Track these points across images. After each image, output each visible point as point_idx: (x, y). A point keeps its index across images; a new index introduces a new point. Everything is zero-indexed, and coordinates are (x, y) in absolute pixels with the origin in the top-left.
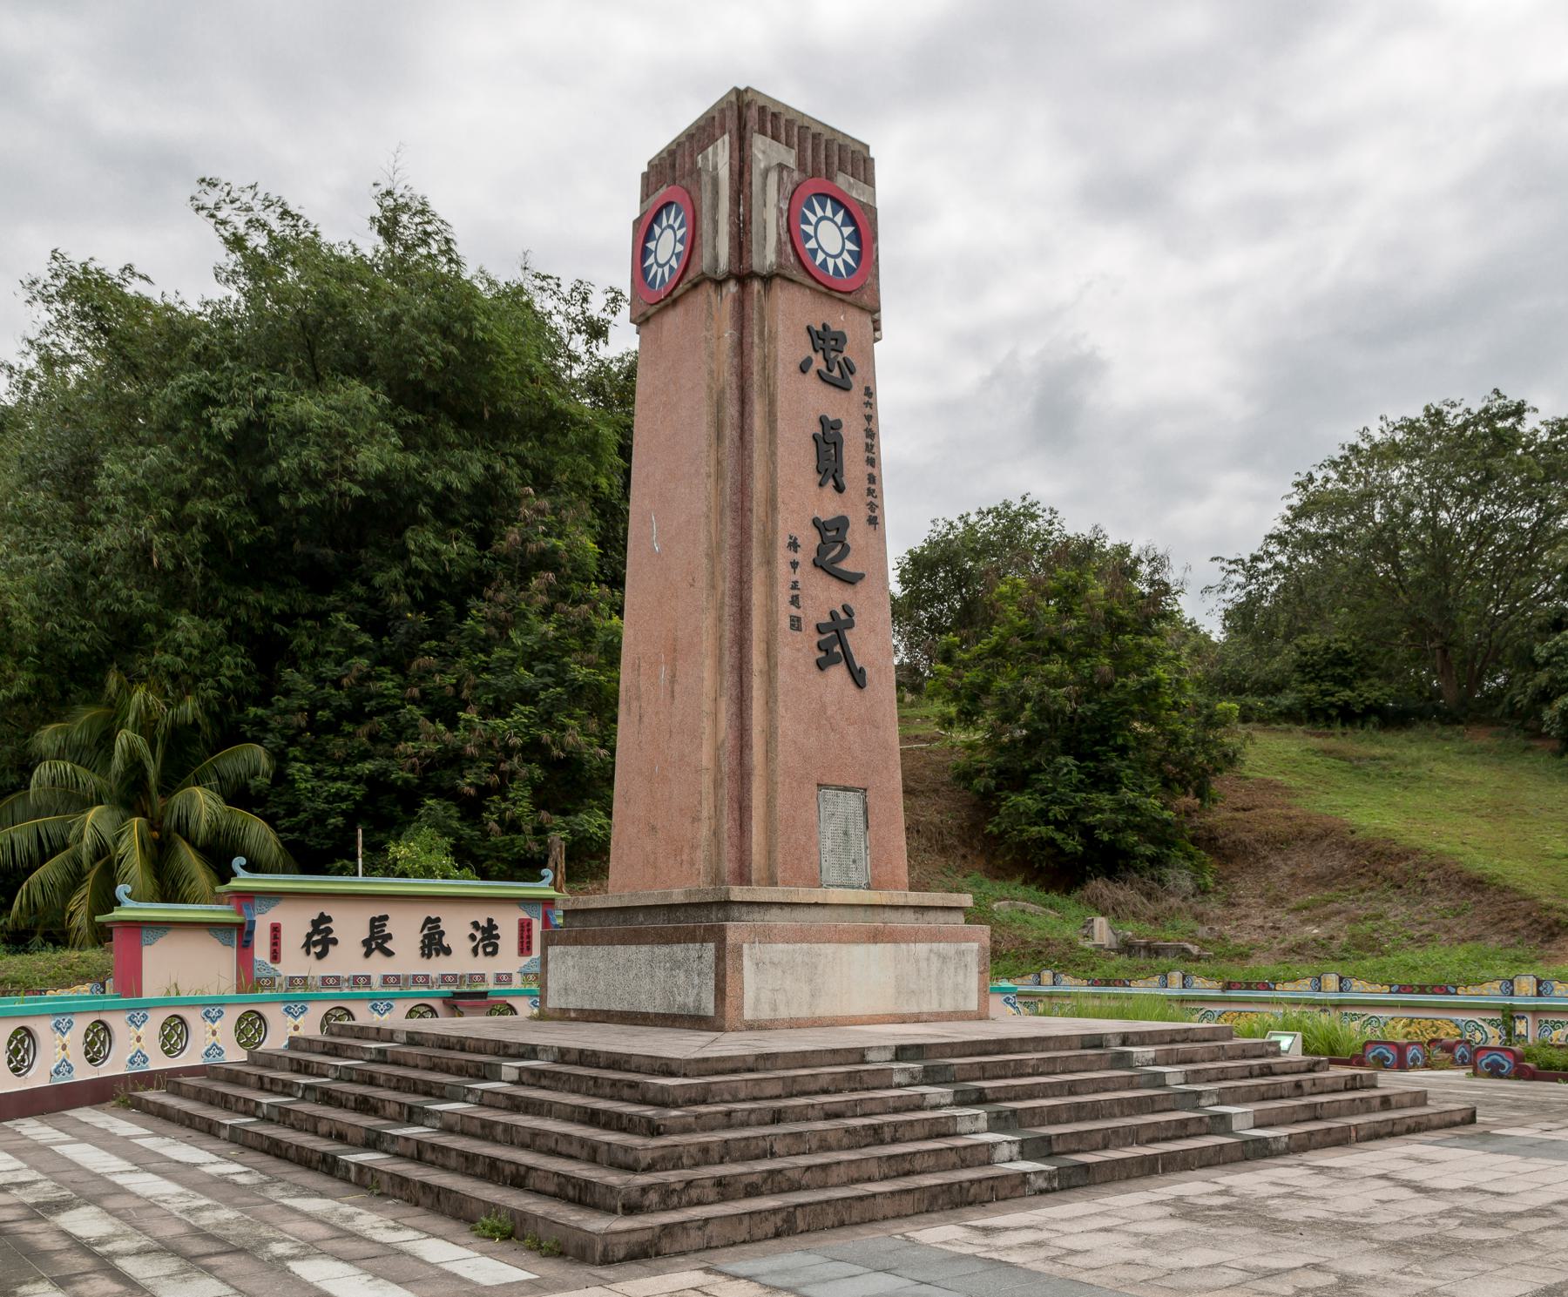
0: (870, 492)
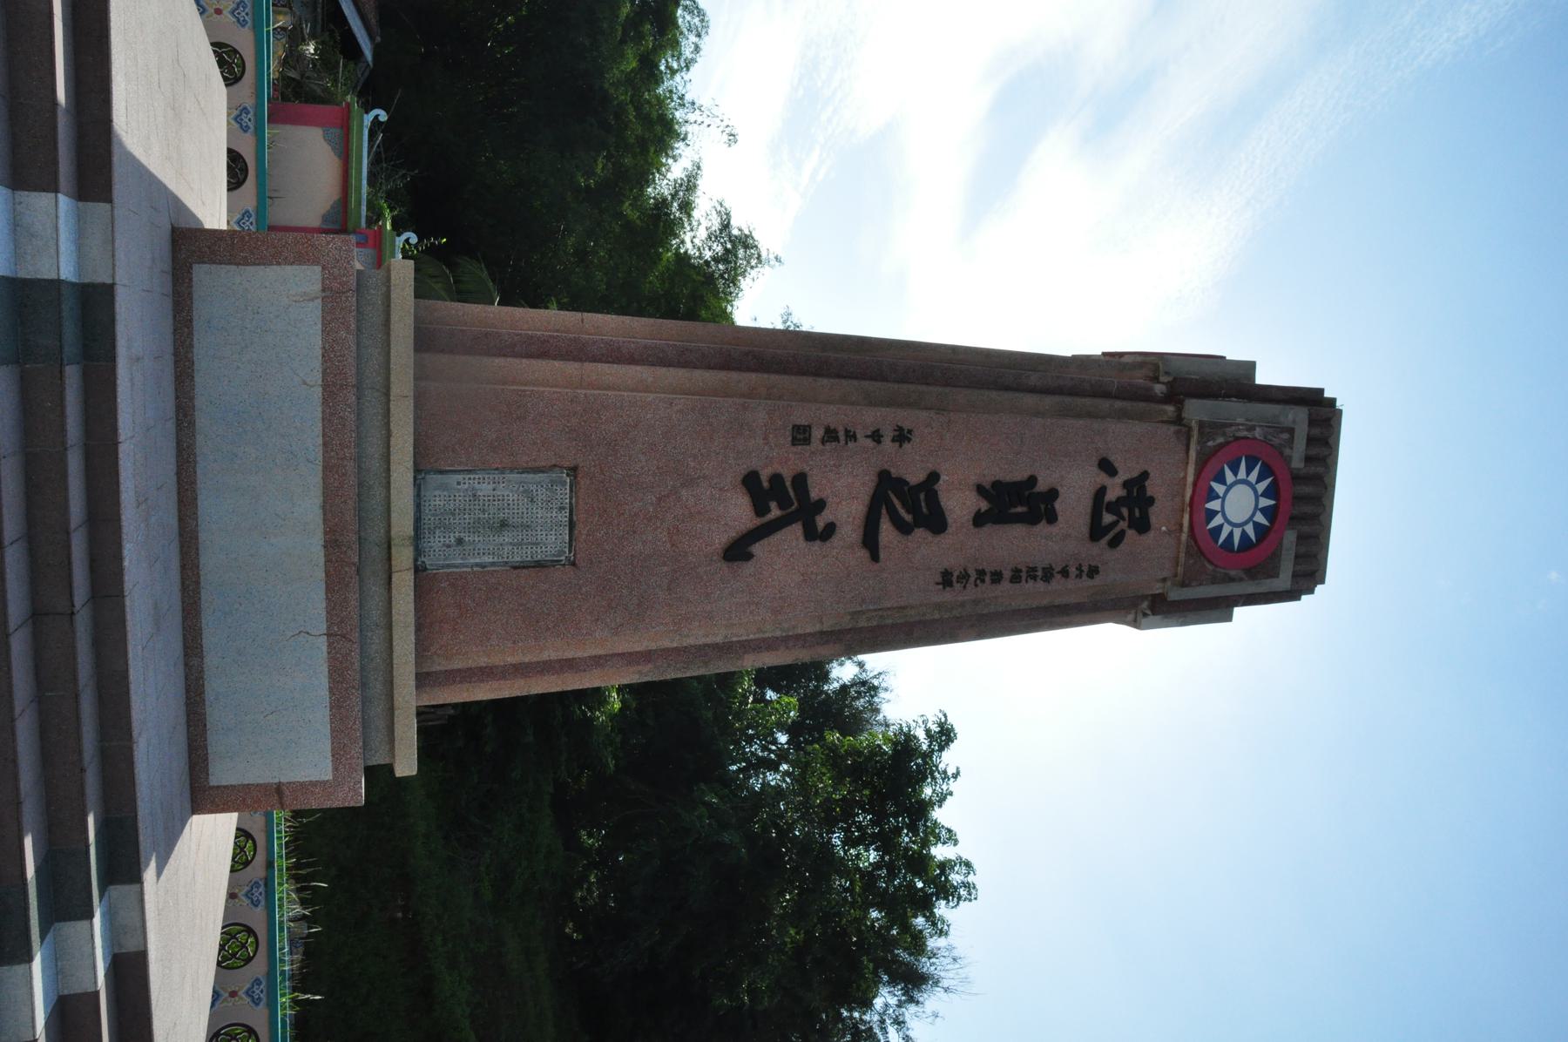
0: (981, 573)
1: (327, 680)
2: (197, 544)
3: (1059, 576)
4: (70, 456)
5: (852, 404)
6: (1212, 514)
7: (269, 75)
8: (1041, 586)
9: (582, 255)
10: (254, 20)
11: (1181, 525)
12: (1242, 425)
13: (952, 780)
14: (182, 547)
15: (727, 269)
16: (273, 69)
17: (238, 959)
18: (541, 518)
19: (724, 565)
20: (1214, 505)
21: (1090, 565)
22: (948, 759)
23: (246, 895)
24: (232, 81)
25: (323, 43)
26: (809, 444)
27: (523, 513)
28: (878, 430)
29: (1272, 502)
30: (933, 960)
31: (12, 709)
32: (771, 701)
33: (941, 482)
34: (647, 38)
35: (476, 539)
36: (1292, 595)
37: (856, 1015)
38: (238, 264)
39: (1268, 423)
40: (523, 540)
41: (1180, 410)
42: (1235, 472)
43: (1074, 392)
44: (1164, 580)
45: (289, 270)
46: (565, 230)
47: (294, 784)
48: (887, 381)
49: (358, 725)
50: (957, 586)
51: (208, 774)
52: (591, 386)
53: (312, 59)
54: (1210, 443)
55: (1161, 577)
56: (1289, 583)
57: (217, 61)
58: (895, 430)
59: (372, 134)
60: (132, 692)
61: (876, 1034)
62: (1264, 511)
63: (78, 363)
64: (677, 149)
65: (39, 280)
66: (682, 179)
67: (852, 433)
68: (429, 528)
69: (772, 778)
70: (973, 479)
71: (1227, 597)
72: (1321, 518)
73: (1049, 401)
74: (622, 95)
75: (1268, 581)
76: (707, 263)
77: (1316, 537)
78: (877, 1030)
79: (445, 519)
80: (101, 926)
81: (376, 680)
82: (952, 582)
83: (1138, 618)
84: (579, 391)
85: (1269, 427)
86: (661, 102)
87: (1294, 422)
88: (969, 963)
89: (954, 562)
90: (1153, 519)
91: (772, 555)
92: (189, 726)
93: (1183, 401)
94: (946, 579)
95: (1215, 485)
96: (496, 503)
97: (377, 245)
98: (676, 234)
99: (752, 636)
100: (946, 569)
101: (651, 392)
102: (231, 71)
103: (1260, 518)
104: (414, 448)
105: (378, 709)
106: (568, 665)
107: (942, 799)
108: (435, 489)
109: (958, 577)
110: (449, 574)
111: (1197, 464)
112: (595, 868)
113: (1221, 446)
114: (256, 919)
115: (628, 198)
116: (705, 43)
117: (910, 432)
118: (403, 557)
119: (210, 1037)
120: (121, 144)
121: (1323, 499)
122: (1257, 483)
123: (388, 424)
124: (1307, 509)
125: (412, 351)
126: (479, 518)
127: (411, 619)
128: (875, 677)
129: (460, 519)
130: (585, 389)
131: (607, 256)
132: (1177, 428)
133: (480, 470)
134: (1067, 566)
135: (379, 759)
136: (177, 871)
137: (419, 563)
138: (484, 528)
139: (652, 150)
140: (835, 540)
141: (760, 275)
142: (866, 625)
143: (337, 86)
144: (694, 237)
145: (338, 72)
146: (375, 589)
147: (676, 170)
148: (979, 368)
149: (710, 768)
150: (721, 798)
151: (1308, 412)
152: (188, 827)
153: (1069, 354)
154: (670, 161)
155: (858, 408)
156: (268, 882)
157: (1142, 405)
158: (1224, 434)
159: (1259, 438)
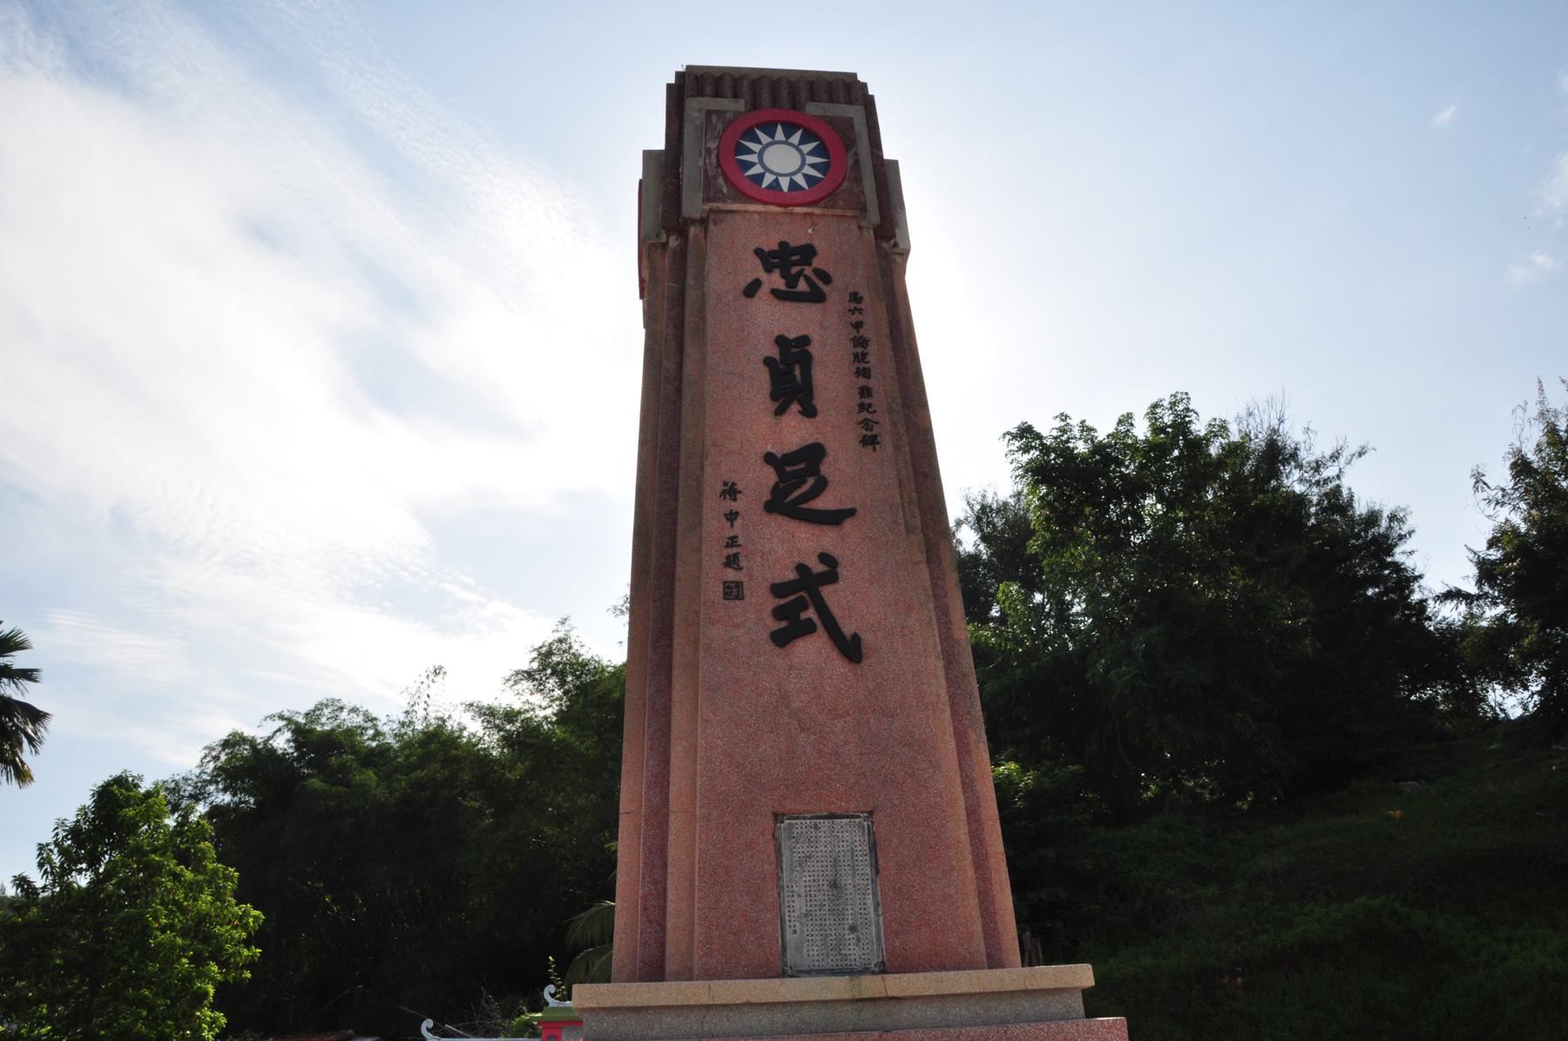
0: (863, 407)
3: (861, 331)
5: (700, 541)
6: (794, 185)
8: (872, 348)
9: (561, 819)
11: (806, 214)
13: (1068, 421)
15: (572, 673)
18: (826, 847)
19: (866, 663)
20: (785, 184)
21: (850, 301)
22: (1046, 428)
26: (742, 583)
27: (822, 866)
28: (725, 515)
30: (1252, 436)
33: (774, 451)
35: (850, 912)
36: (869, 104)
37: (1313, 510)
41: (693, 221)
42: (751, 165)
44: (860, 228)
46: (537, 837)
49: (1044, 1026)
50: (876, 431)
54: (725, 190)
55: (857, 230)
58: (725, 498)
61: (1331, 489)
62: (788, 135)
64: (453, 727)
66: (483, 721)
67: (730, 542)
68: (841, 960)
70: (769, 419)
72: (793, 79)
73: (690, 349)
74: (401, 784)
75: (856, 127)
82: (871, 436)
83: (900, 251)
84: (698, 813)
85: (706, 135)
86: (408, 745)
87: (700, 111)
88: (1252, 399)
89: (851, 436)
90: (802, 241)
93: (684, 218)
96: (813, 893)
99: (936, 632)
100: (860, 442)
103: (795, 139)
104: (761, 978)
105: (1026, 1006)
106: (973, 813)
107: (1086, 429)
108: (802, 957)
111: (745, 202)
113: (727, 180)
115: (504, 774)
116: (348, 702)
117: (725, 484)
118: (872, 986)
123: (738, 1006)
124: (784, 94)
127: (935, 975)
128: (972, 509)
131: (562, 794)
132: (711, 224)
133: (780, 910)
134: (851, 324)
135: (1078, 1004)
137: (877, 969)
139: (454, 752)
140: (829, 549)
146: (905, 1013)
147: (474, 727)
150: (1101, 656)
151: (690, 99)
154: (465, 733)
155: (704, 535)
157: (690, 260)
158: (715, 178)
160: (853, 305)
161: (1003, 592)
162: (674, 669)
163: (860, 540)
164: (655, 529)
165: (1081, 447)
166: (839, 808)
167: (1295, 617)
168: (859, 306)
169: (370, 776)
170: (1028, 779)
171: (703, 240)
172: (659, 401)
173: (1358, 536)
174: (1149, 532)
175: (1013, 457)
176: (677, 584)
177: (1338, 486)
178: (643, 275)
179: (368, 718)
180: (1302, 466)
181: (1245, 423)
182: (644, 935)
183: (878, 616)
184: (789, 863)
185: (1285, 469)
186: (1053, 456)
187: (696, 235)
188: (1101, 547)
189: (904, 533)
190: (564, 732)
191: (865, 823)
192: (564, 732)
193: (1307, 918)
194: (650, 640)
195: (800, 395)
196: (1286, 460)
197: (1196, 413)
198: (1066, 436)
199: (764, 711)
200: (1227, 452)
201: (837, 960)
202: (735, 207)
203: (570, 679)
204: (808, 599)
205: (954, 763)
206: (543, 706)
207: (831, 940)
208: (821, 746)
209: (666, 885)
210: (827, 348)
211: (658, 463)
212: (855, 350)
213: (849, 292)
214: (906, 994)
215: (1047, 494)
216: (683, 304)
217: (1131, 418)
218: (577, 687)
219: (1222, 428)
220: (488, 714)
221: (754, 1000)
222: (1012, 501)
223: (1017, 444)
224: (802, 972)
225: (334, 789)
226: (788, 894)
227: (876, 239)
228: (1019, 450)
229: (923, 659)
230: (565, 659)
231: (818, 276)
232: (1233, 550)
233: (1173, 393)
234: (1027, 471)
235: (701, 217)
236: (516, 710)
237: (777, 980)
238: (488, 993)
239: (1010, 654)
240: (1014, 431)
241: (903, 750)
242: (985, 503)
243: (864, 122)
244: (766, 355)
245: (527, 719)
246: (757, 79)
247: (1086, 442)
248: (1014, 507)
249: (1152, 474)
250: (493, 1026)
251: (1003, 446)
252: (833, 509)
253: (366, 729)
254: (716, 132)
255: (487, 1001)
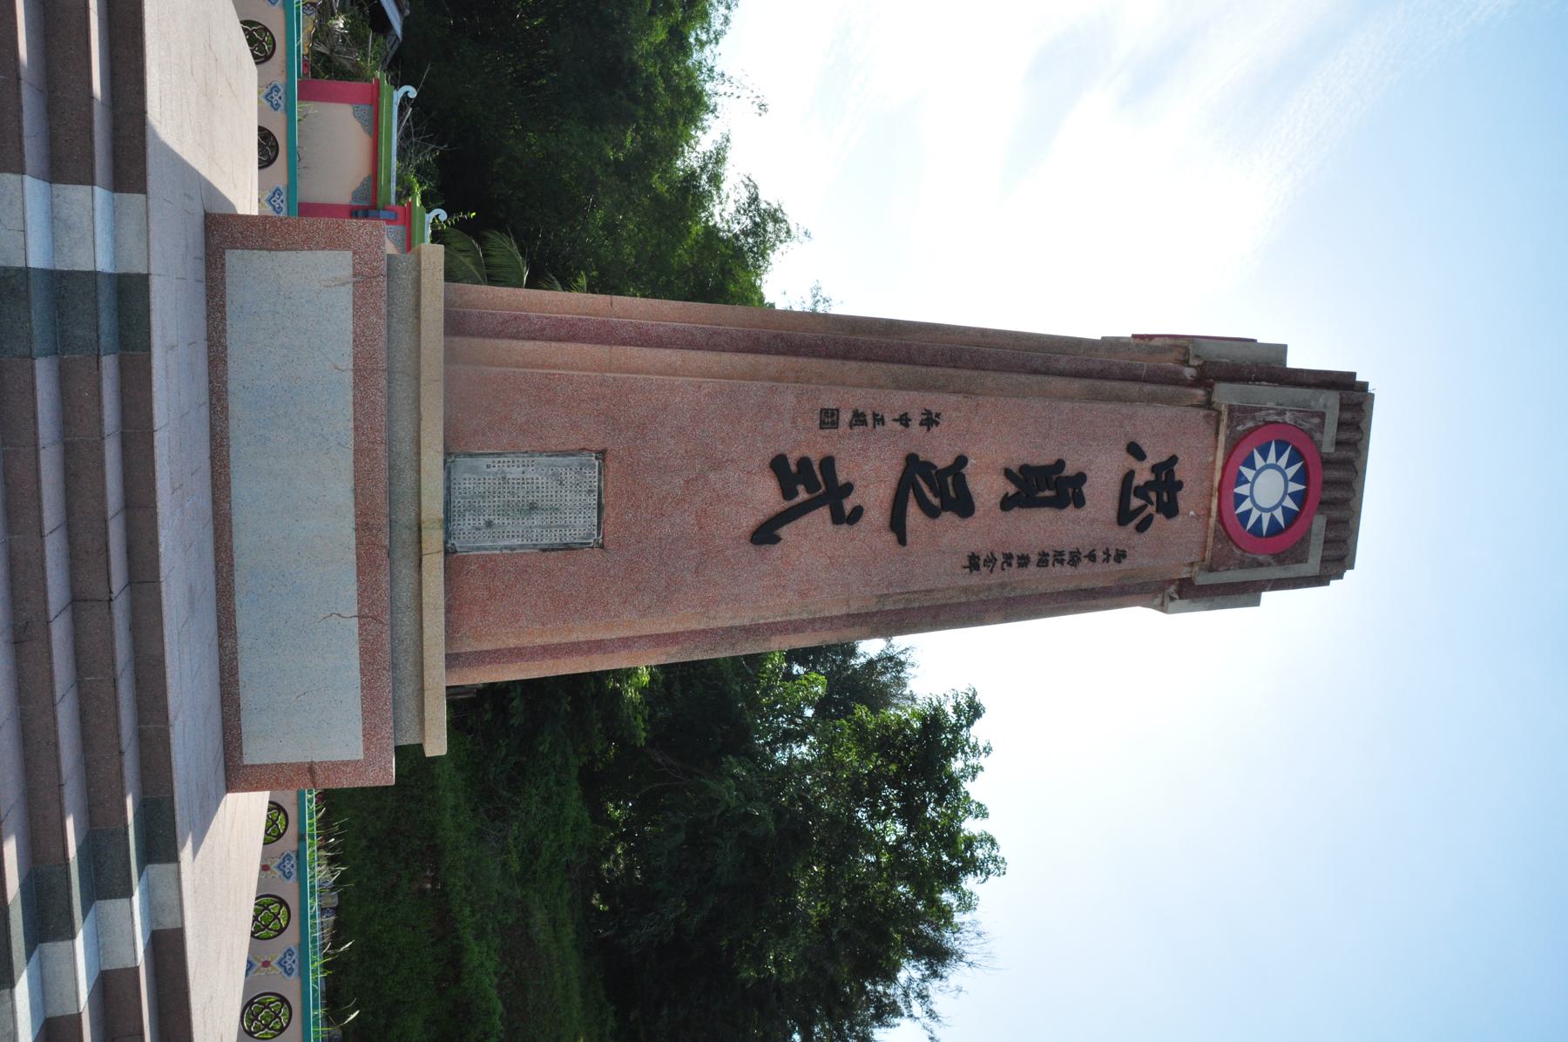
0: (1008, 557)
1: (358, 662)
2: (231, 526)
3: (1086, 561)
4: (107, 447)
5: (881, 387)
6: (1240, 499)
7: (299, 51)
8: (1068, 570)
9: (610, 228)
10: (286, 106)
11: (1209, 510)
12: (1272, 409)
13: (984, 754)
14: (216, 529)
15: (756, 243)
16: (302, 43)
17: (271, 930)
18: (571, 500)
19: (751, 548)
20: (1243, 490)
21: (1117, 550)
22: (978, 732)
23: (278, 867)
24: (263, 59)
25: (352, 17)
26: (837, 428)
27: (552, 496)
28: (906, 414)
29: (1302, 487)
30: (957, 935)
31: (53, 693)
32: (799, 675)
33: (969, 466)
34: (676, 10)
35: (506, 522)
36: (1321, 580)
37: (880, 988)
38: (270, 250)
39: (1299, 407)
40: (551, 522)
41: (1209, 394)
42: (1265, 457)
43: (1104, 375)
44: (1192, 564)
45: (320, 255)
46: (594, 203)
47: (326, 762)
48: (917, 364)
49: (389, 706)
50: (984, 569)
51: (242, 754)
52: (619, 369)
53: (341, 34)
54: (1240, 428)
55: (1189, 561)
56: (1318, 568)
57: (247, 40)
58: (923, 414)
59: (402, 109)
60: (168, 676)
61: (899, 1007)
62: (1293, 496)
63: (114, 353)
64: (707, 120)
65: (76, 272)
66: (711, 152)
67: (879, 417)
68: (459, 511)
69: (801, 751)
70: (1002, 463)
71: (1255, 582)
72: (1351, 503)
73: (1077, 385)
74: (651, 66)
75: (1297, 566)
76: (736, 236)
77: (1346, 522)
78: (901, 1004)
79: (475, 502)
80: (140, 904)
81: (407, 660)
82: (979, 565)
83: (1165, 603)
84: (608, 375)
85: (1300, 411)
86: (690, 76)
87: (1325, 406)
88: (993, 938)
89: (981, 546)
90: (1181, 504)
91: (800, 538)
92: (223, 706)
93: (1213, 384)
94: (973, 563)
95: (1244, 470)
96: (525, 486)
97: (406, 218)
98: (705, 207)
99: (779, 619)
100: (973, 553)
101: (679, 375)
102: (262, 50)
103: (1289, 503)
104: (445, 432)
105: (408, 689)
106: (598, 646)
107: (975, 771)
108: (464, 472)
109: (985, 560)
110: (478, 556)
111: (1226, 448)
112: (622, 840)
113: (1250, 431)
114: (289, 891)
115: (657, 171)
116: (734, 15)
117: (938, 415)
118: (433, 540)
119: (245, 1003)
120: (155, 135)
121: (1353, 484)
122: (1286, 468)
123: (418, 408)
124: (1338, 494)
125: (443, 335)
126: (509, 501)
127: (441, 602)
128: (901, 652)
129: (489, 502)
130: (613, 372)
131: (636, 229)
132: (1206, 412)
133: (510, 453)
134: (1094, 550)
135: (409, 739)
136: (213, 848)
137: (449, 545)
138: (513, 510)
139: (681, 122)
140: (863, 523)
141: (789, 250)
142: (893, 608)
143: (366, 61)
144: (723, 210)
145: (367, 47)
146: (406, 572)
147: (704, 141)
148: (1008, 351)
149: (738, 741)
150: (749, 771)
151: (1338, 397)
152: (222, 806)
153: (1096, 335)
154: (699, 133)
155: (887, 392)
156: (300, 854)
157: (1171, 389)
158: (1254, 418)
159: (1289, 422)
160: (1113, 553)
161: (816, 679)
162: (753, 356)
163: (873, 548)
164: (895, 341)
165: (957, 765)
166: (608, 515)
167: (777, 963)
168: (1112, 559)
169: (660, 35)
170: (631, 693)
171: (1189, 403)
172: (1026, 351)
173: (851, 1029)
174: (869, 826)
175: (951, 697)
176: (839, 362)
177: (902, 1015)
178: (1156, 339)
179: (719, 34)
180: (924, 981)
181: (970, 929)
182: (490, 317)
183: (798, 563)
184: (555, 463)
185: (922, 965)
186: (949, 736)
187: (1195, 396)
188: (855, 780)
189: (879, 593)
190: (697, 234)
191: (592, 541)
192: (697, 234)
193: (485, 954)
194: (784, 332)
195: (1024, 495)
196: (931, 966)
197: (985, 880)
198: (969, 751)
199: (707, 444)
200: (943, 909)
201: (460, 507)
202: (1222, 438)
203: (750, 240)
204: (817, 493)
205: (647, 631)
206: (723, 213)
207: (479, 502)
208: (670, 500)
209: (539, 340)
210: (1071, 524)
211: (963, 347)
212: (1067, 553)
213: (1127, 550)
214: (424, 574)
215: (912, 729)
216: (1123, 379)
217: (983, 816)
218: (741, 248)
219: (967, 906)
220: (719, 158)
221: (423, 424)
222: (907, 692)
223: (963, 702)
224: (449, 473)
225: (553, 277)
226: (526, 461)
227: (1179, 579)
228: (957, 704)
229: (751, 605)
230: (770, 235)
231: (1144, 519)
232: (846, 907)
233: (1006, 861)
234: (935, 709)
235: (1214, 402)
236: (721, 185)
237: (442, 446)
238: (441, 151)
239: (755, 682)
240: (977, 700)
241: (663, 581)
242: (907, 666)
243: (1302, 575)
244: (1067, 462)
245: (712, 197)
246: (1354, 466)
247: (962, 770)
248: (901, 694)
249: (926, 833)
250: (409, 154)
251: (962, 688)
252: (907, 523)
253: (708, 32)
254: (1301, 422)
255: (433, 150)
